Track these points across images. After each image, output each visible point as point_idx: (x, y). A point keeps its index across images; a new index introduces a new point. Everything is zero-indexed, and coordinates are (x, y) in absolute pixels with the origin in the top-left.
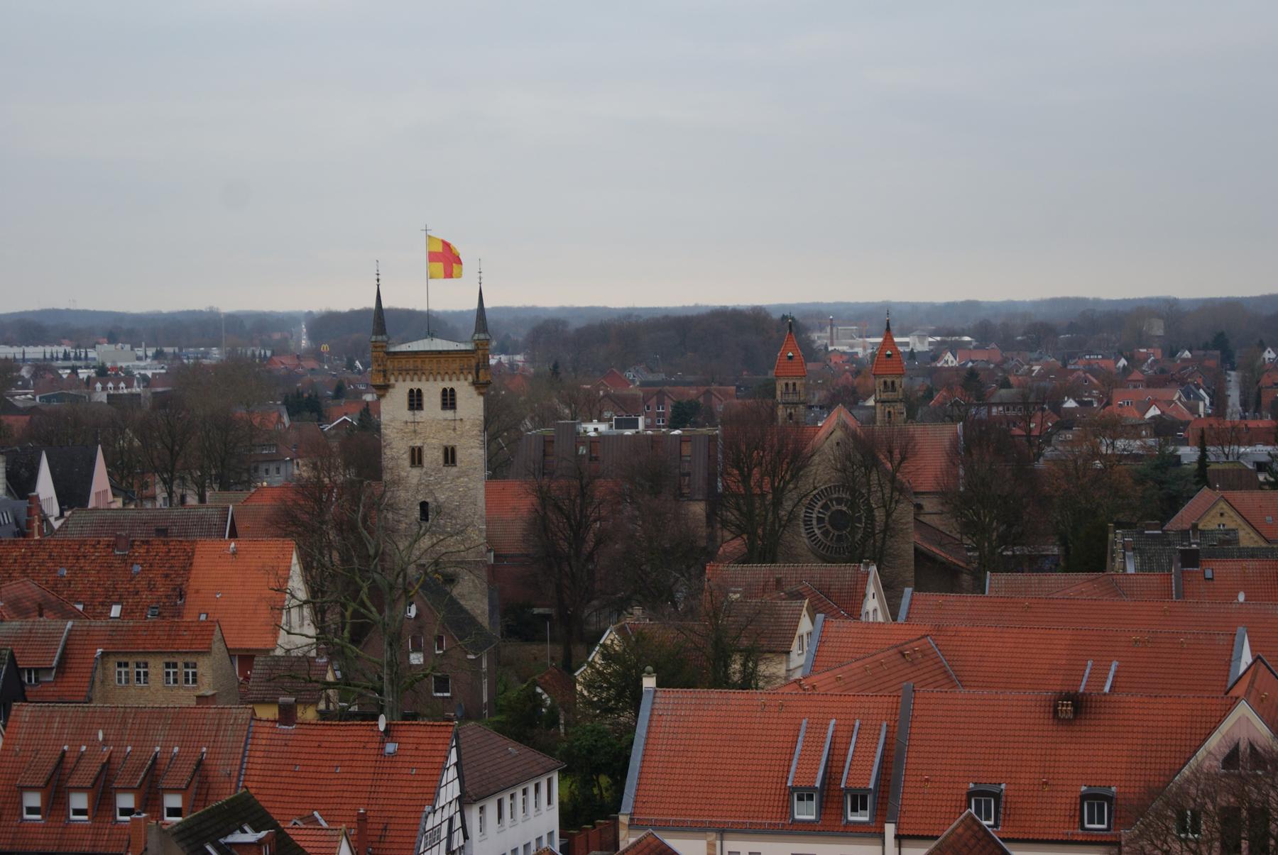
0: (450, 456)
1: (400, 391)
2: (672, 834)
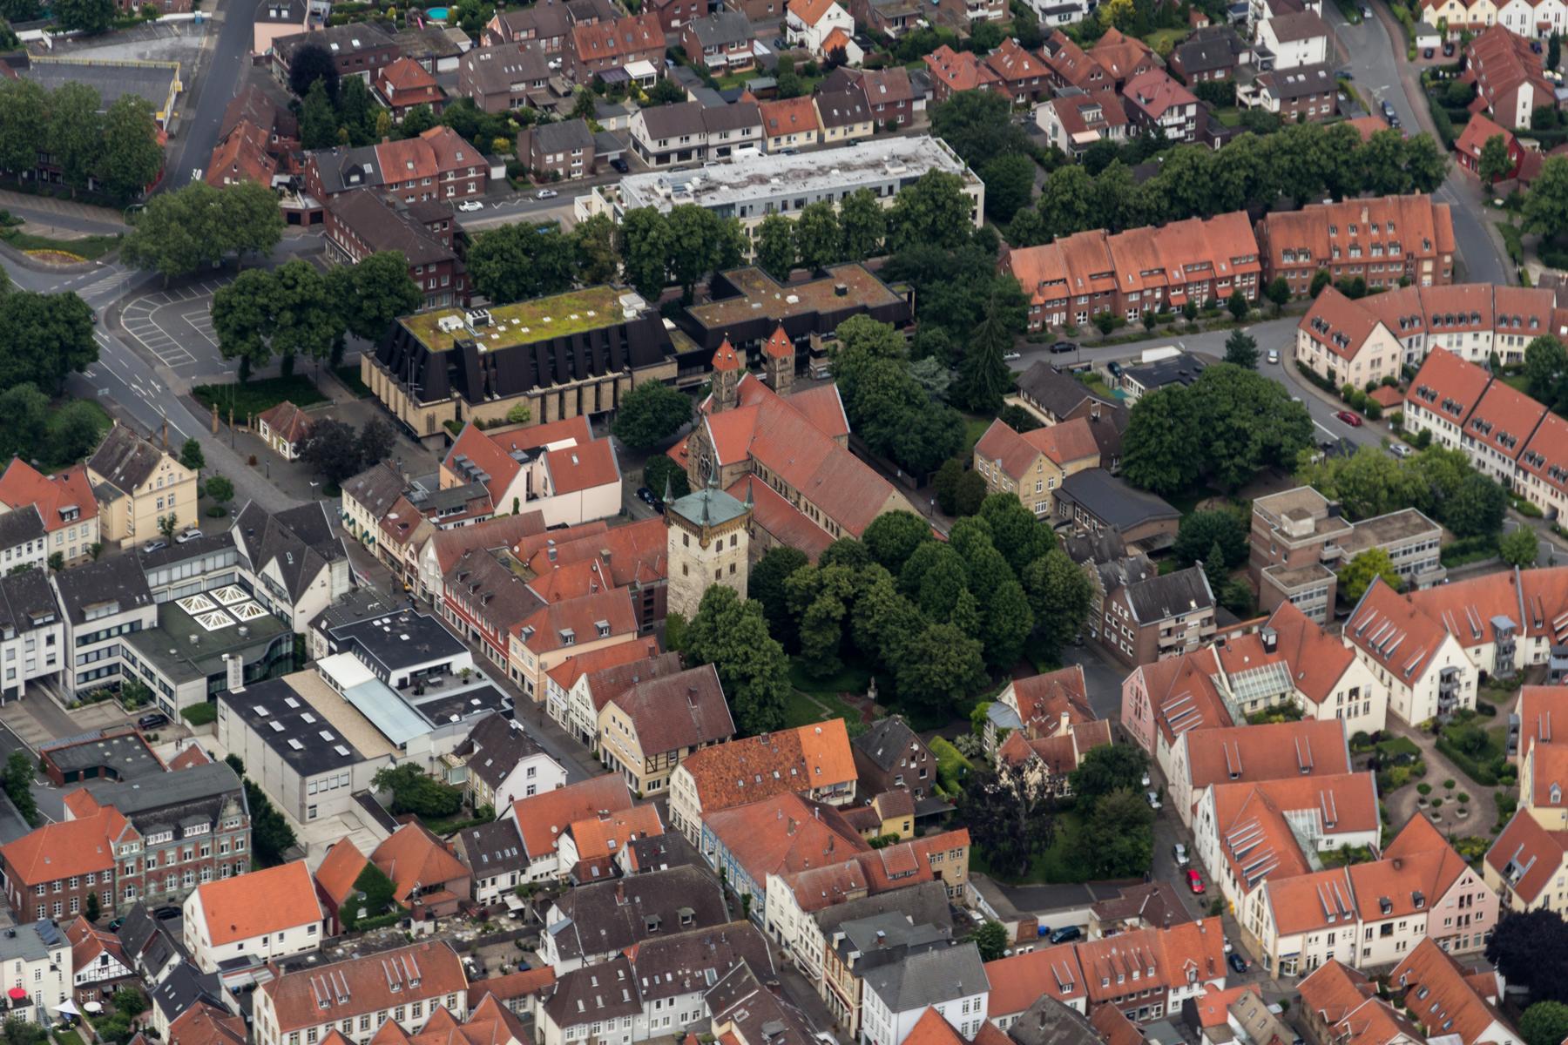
0: (733, 568)
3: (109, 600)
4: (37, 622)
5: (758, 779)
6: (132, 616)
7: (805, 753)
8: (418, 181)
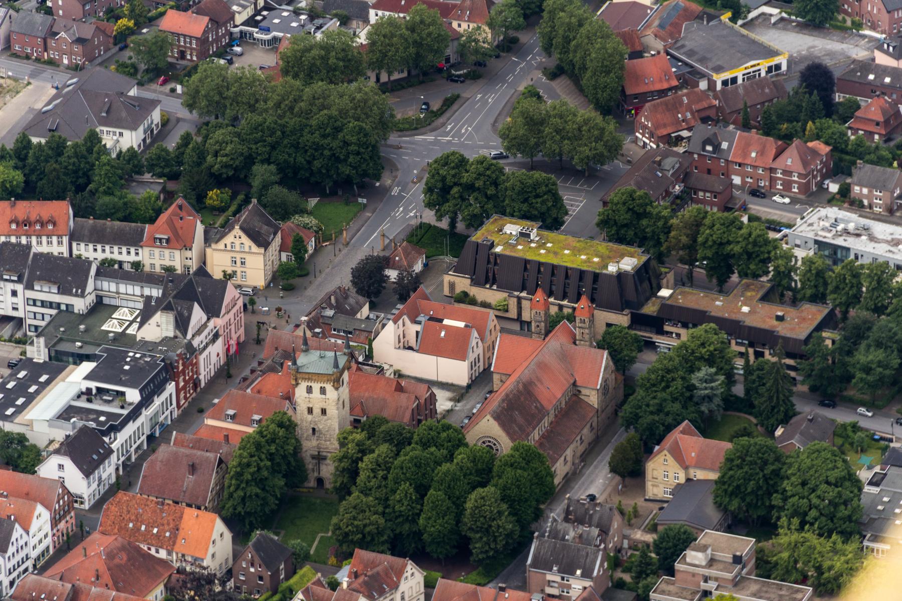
1: (303, 385)
2: (26, 410)
3: (55, 283)
4: (5, 277)
5: (143, 528)
6: (65, 300)
7: (182, 526)
8: (755, 167)
